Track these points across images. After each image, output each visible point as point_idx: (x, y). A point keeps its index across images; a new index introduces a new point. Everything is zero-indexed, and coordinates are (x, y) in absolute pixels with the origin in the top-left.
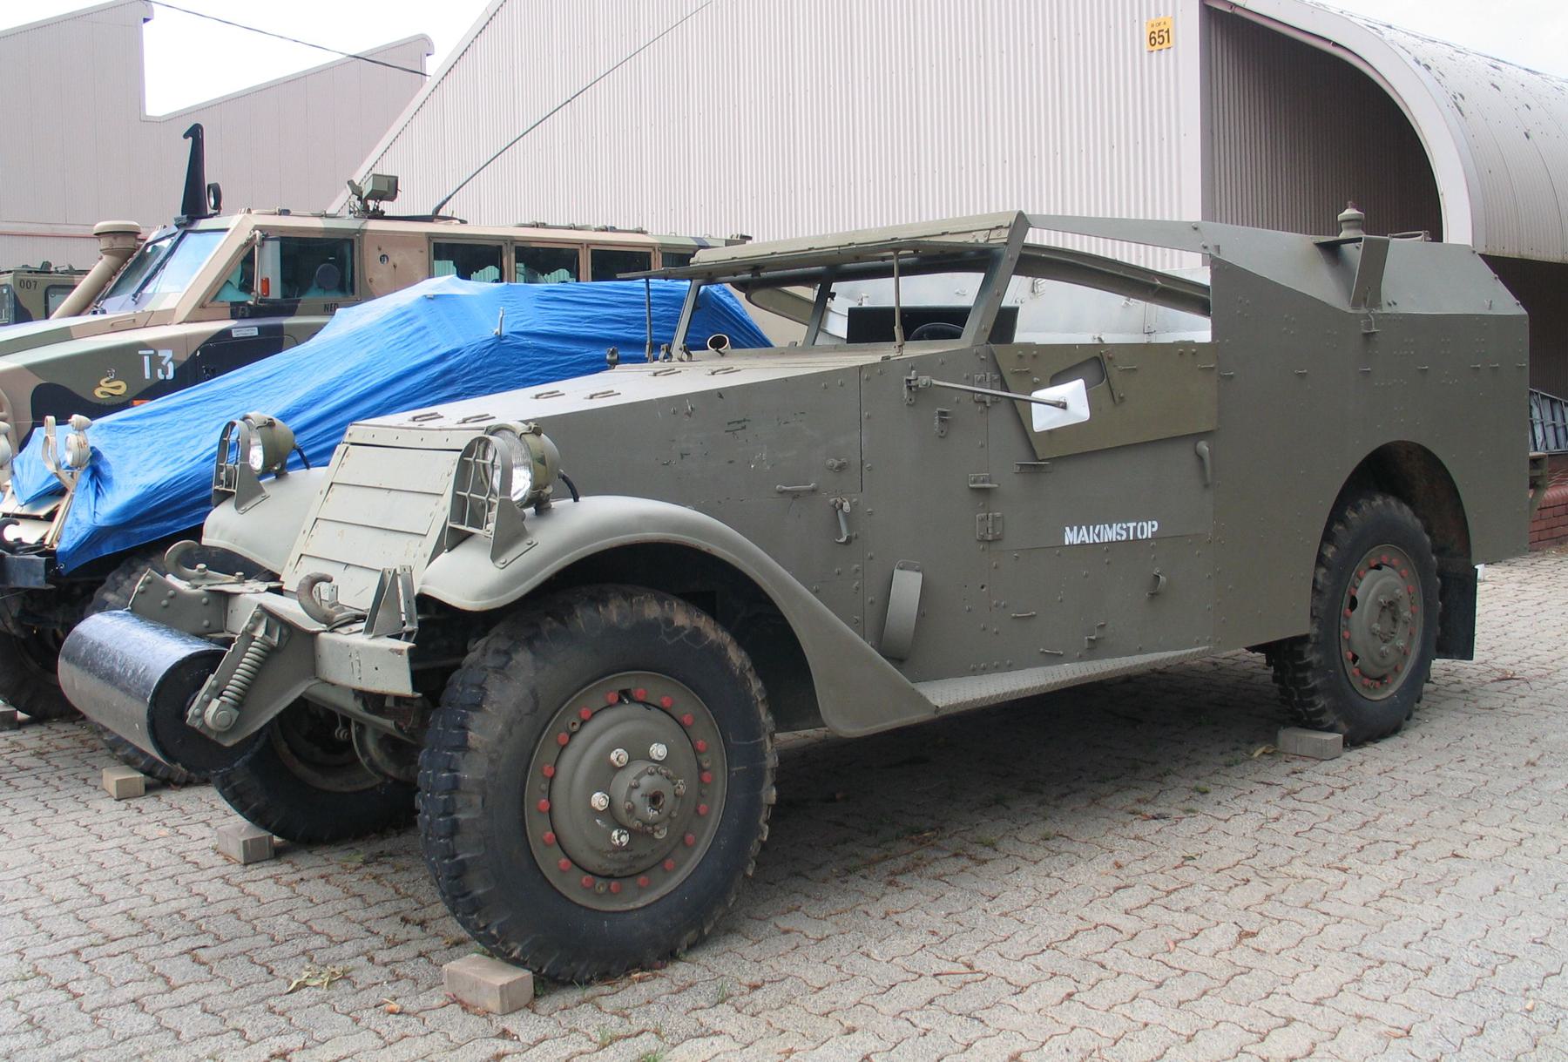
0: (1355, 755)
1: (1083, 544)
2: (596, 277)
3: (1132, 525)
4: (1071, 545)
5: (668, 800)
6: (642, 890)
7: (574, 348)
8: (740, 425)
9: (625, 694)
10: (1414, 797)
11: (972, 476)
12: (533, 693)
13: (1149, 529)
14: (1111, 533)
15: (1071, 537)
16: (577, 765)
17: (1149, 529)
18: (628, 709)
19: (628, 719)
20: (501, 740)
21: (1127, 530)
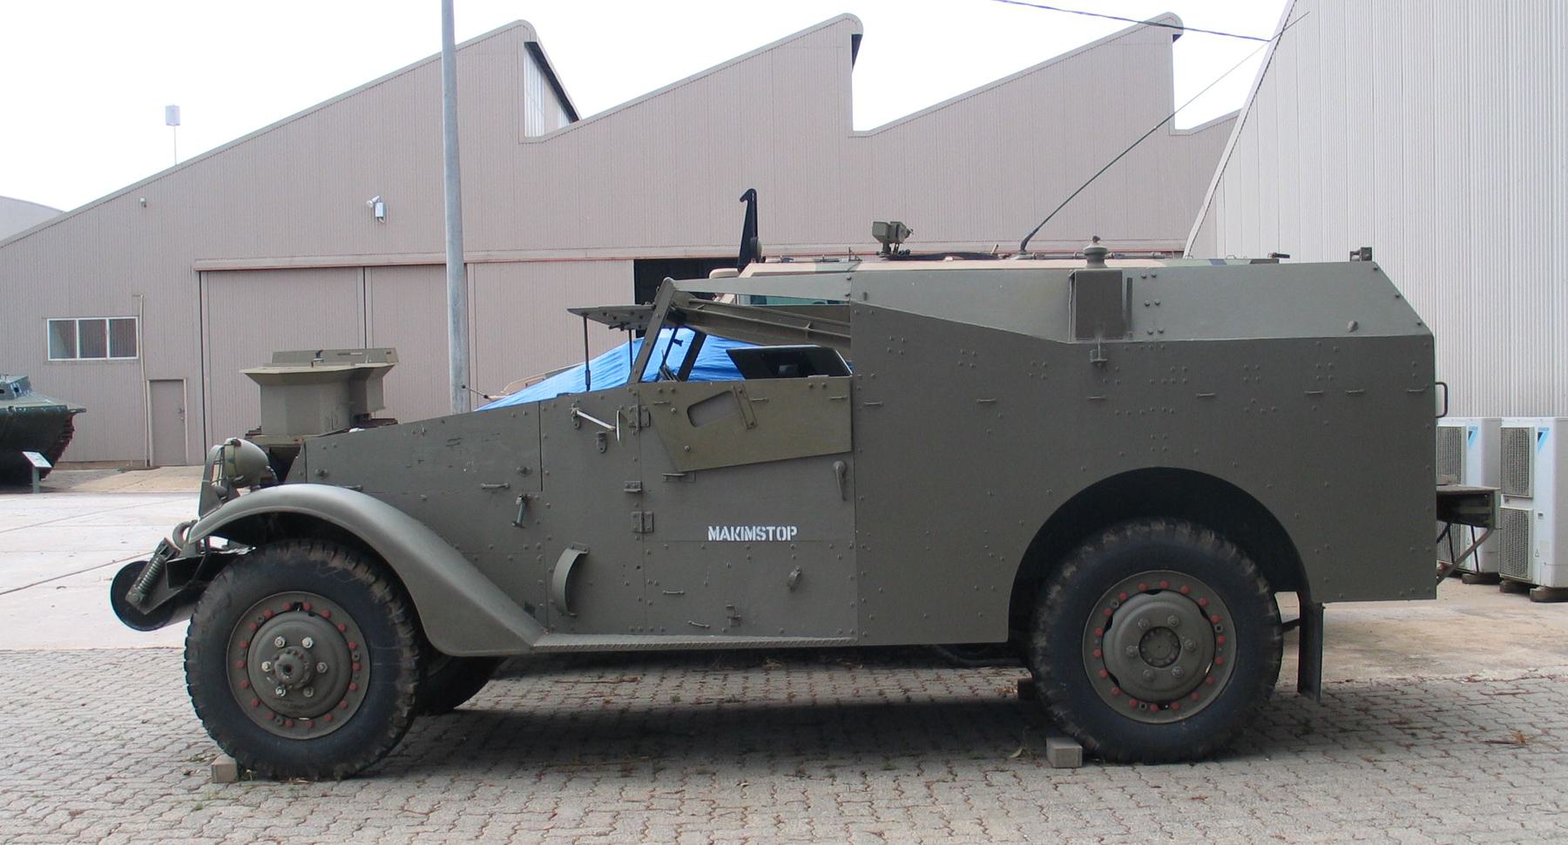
0: (1092, 773)
1: (725, 541)
2: (82, 356)
3: (771, 529)
4: (714, 541)
5: (296, 671)
6: (1197, 702)
7: (715, 376)
8: (455, 441)
9: (295, 607)
10: (643, 832)
11: (626, 482)
12: (229, 596)
13: (788, 533)
14: (750, 534)
15: (713, 534)
16: (1121, 621)
17: (788, 533)
18: (297, 615)
19: (296, 621)
20: (209, 620)
21: (767, 532)
